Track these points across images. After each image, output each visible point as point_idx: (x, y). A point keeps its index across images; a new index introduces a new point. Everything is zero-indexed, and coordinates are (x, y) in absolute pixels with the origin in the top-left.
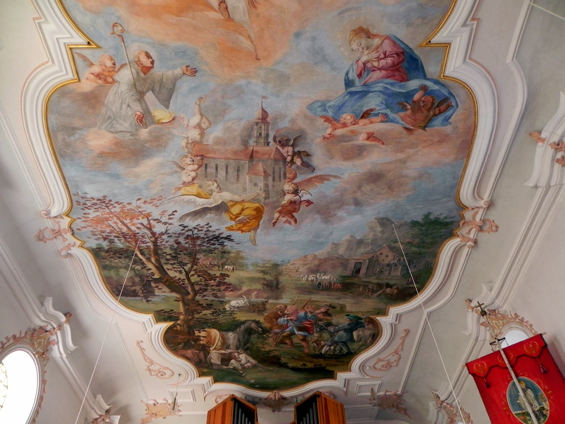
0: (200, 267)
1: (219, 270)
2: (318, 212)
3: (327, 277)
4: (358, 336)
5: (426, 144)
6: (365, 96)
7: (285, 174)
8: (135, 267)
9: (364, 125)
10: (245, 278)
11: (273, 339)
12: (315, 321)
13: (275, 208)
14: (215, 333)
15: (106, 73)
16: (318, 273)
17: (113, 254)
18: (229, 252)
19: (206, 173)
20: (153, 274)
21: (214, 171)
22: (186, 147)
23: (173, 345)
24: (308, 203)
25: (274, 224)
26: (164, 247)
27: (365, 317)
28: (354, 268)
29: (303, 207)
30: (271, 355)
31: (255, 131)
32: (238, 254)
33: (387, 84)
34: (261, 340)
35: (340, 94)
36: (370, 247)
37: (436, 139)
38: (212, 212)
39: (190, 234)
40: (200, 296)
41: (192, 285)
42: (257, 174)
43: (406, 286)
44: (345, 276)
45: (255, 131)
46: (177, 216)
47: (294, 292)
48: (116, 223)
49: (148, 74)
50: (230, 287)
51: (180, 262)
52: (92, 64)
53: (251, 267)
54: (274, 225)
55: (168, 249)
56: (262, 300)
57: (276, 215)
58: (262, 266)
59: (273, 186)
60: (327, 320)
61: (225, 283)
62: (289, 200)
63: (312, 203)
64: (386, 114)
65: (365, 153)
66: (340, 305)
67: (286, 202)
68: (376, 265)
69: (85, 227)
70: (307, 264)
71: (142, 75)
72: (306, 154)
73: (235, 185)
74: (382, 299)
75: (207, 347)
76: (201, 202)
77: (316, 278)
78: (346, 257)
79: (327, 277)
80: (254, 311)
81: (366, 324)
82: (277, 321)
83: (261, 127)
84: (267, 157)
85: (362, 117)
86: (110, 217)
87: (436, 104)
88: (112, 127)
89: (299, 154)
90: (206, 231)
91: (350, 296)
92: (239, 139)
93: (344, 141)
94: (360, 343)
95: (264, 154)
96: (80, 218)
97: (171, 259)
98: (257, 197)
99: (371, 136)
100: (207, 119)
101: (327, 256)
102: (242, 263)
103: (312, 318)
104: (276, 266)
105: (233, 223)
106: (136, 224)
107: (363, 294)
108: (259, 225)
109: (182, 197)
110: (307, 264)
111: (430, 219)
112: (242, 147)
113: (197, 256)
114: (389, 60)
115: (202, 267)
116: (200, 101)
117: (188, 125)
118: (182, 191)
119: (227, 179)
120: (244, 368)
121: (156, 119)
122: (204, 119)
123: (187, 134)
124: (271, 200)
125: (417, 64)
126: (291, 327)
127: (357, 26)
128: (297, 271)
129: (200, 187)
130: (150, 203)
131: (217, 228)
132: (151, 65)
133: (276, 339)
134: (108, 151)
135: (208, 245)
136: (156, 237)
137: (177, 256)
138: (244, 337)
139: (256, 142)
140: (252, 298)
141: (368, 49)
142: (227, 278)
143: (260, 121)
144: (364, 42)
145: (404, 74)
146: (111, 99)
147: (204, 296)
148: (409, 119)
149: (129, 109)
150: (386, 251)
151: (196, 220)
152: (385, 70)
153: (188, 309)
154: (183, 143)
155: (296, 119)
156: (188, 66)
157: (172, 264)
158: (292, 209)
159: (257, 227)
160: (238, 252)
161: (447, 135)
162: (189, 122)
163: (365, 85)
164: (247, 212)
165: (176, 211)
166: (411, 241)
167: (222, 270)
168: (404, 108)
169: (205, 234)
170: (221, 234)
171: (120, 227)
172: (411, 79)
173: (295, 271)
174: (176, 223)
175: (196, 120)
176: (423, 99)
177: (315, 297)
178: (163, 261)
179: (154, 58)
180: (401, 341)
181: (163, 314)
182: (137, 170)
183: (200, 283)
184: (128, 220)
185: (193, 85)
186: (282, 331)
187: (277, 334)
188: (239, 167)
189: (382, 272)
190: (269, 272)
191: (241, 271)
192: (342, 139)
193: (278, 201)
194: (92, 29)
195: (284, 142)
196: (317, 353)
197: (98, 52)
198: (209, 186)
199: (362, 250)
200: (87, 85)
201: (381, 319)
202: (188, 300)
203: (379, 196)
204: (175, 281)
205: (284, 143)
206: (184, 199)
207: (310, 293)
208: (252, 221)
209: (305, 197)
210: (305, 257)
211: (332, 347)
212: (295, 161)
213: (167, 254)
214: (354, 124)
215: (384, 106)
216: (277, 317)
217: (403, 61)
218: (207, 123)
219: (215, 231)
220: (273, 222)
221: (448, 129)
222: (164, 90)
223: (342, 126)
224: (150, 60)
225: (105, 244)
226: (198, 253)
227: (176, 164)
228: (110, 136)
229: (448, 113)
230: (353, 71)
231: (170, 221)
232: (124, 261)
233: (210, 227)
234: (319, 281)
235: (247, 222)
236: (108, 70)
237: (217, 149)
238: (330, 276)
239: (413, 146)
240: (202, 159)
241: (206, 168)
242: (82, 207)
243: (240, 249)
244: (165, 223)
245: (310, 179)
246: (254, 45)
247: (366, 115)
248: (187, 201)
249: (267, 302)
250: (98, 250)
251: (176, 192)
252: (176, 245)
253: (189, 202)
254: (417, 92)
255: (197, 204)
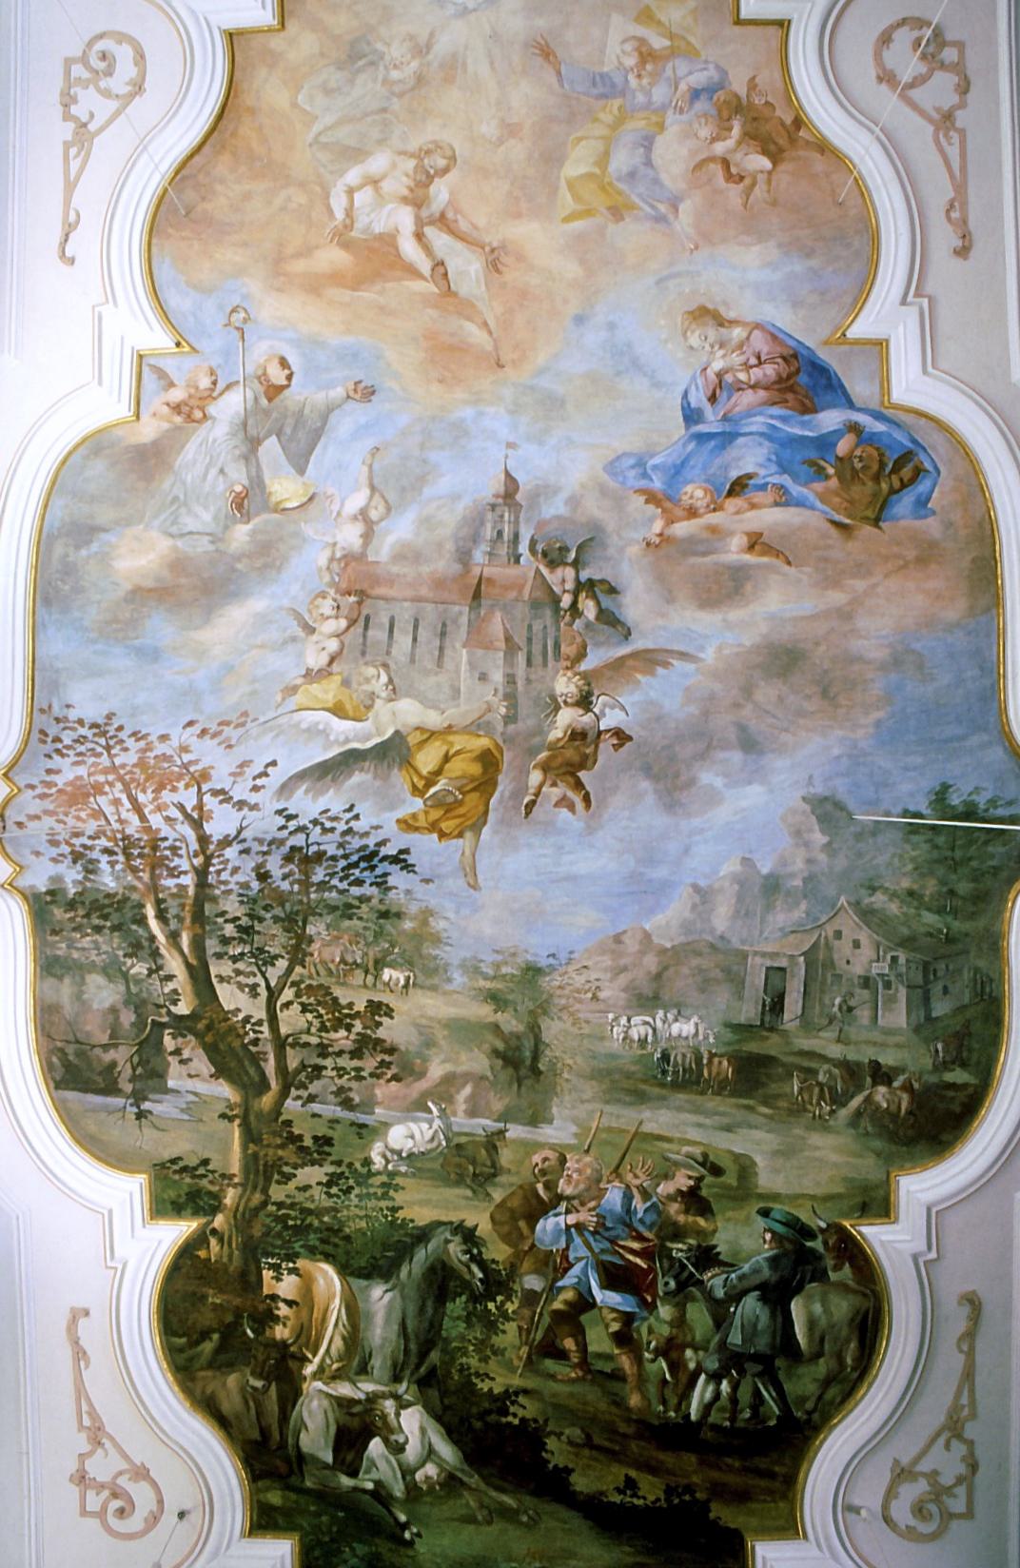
0: (313, 970)
1: (365, 986)
2: (648, 771)
3: (684, 1028)
4: (812, 1324)
5: (890, 566)
6: (731, 442)
7: (557, 646)
8: (133, 966)
9: (738, 513)
10: (439, 1022)
11: (520, 1328)
12: (657, 1236)
13: (532, 752)
14: (327, 1278)
15: (194, 402)
16: (657, 1007)
17: (83, 917)
18: (399, 915)
19: (364, 644)
20: (174, 998)
21: (383, 636)
22: (328, 568)
23: (183, 1340)
24: (619, 739)
25: (530, 807)
26: (224, 892)
27: (823, 1225)
28: (765, 991)
29: (606, 745)
30: (510, 1419)
31: (489, 526)
32: (425, 923)
33: (772, 417)
34: (478, 1335)
35: (676, 437)
36: (803, 906)
37: (911, 554)
38: (367, 764)
39: (298, 845)
40: (299, 1097)
41: (281, 1044)
42: (489, 646)
43: (933, 1079)
44: (740, 1025)
45: (489, 526)
46: (277, 777)
47: (589, 1089)
48: (117, 802)
49: (277, 401)
50: (395, 1063)
51: (258, 949)
52: (172, 385)
53: (459, 979)
54: (527, 814)
55: (233, 897)
56: (487, 1122)
57: (535, 777)
58: (491, 972)
59: (528, 681)
60: (700, 1233)
61: (379, 1041)
62: (569, 726)
63: (630, 738)
64: (782, 487)
65: (748, 587)
66: (737, 1158)
67: (560, 735)
68: (829, 981)
69: (37, 817)
70: (625, 969)
71: (264, 402)
72: (607, 586)
73: (432, 680)
74: (867, 1134)
75: (293, 1356)
76: (346, 733)
77: (654, 1030)
78: (735, 943)
79: (684, 1028)
80: (460, 1181)
81: (830, 1262)
82: (533, 1229)
83: (502, 516)
84: (513, 594)
85: (731, 493)
86: (108, 782)
87: (890, 466)
88: (174, 523)
89: (588, 587)
90: (345, 833)
91: (765, 1116)
92: (450, 546)
93: (695, 554)
94: (822, 1368)
95: (506, 588)
96: (32, 787)
97: (234, 939)
98: (485, 718)
99: (755, 542)
100: (383, 497)
101: (682, 939)
102: (435, 958)
103: (648, 1220)
104: (533, 972)
105: (418, 804)
106: (166, 807)
107: (805, 1110)
108: (486, 813)
109: (297, 716)
110: (625, 969)
111: (949, 805)
112: (457, 568)
113: (310, 930)
114: (770, 370)
115: (318, 974)
116: (373, 455)
117: (339, 514)
118: (299, 699)
119: (413, 661)
120: (413, 1491)
121: (274, 499)
122: (377, 497)
123: (334, 536)
124: (520, 726)
125: (829, 378)
126: (582, 1273)
127: (693, 306)
128: (595, 997)
129: (346, 683)
130: (214, 736)
131: (375, 823)
132: (285, 383)
133: (529, 1331)
134: (149, 583)
135: (344, 885)
136: (208, 853)
137: (252, 927)
138: (422, 1310)
139: (490, 554)
140: (455, 1114)
141: (721, 347)
142: (385, 1020)
143: (500, 501)
144: (712, 333)
145: (806, 397)
146: (190, 456)
147: (312, 1099)
148: (837, 500)
149: (221, 478)
150: (849, 924)
151: (321, 792)
152: (766, 388)
153: (255, 1156)
154: (323, 560)
155: (582, 496)
156: (360, 382)
157: (235, 959)
158: (576, 759)
159: (482, 820)
160: (427, 914)
161: (933, 545)
162: (342, 505)
163: (725, 418)
164: (456, 767)
165: (274, 763)
166: (915, 887)
167: (375, 985)
168: (820, 473)
169: (341, 845)
170: (383, 843)
171: (124, 815)
172: (823, 409)
173: (590, 995)
174: (268, 804)
175: (357, 501)
176: (858, 453)
177: (657, 1119)
178: (212, 945)
179: (294, 369)
180: (959, 1360)
181: (177, 1177)
182: (204, 635)
183: (305, 1038)
184: (149, 791)
185: (363, 420)
186: (551, 1288)
187: (531, 1298)
188: (444, 625)
189: (850, 1009)
190: (510, 997)
191: (429, 993)
192: (690, 547)
193: (540, 731)
194: (191, 319)
195: (555, 555)
196: (672, 1414)
197: (190, 363)
198: (368, 680)
199: (782, 917)
200: (148, 430)
201: (874, 1234)
202: (260, 1115)
203: (801, 721)
204: (232, 1029)
205: (554, 557)
206: (300, 722)
207: (640, 1098)
208: (469, 797)
209: (611, 720)
210: (618, 939)
211: (725, 1386)
212: (580, 606)
213: (227, 917)
214: (715, 510)
215: (774, 468)
216: (537, 1209)
217: (798, 371)
218: (382, 508)
219: (366, 834)
220: (525, 801)
221: (932, 526)
222: (301, 435)
223: (685, 513)
224: (287, 372)
225: (71, 877)
226: (314, 914)
227: (299, 617)
228: (164, 544)
229: (922, 487)
230: (697, 388)
231: (253, 798)
232: (110, 944)
233: (357, 817)
234: (663, 1044)
235: (456, 801)
236: (198, 395)
237: (398, 575)
238: (697, 1024)
239: (861, 570)
240: (360, 603)
241: (366, 627)
242: (49, 747)
243: (433, 903)
244: (241, 804)
245: (622, 659)
246: (495, 340)
247: (737, 488)
248: (308, 730)
249: (501, 1133)
250: (48, 898)
251: (284, 699)
252: (255, 885)
253: (314, 732)
254: (842, 436)
255: (332, 738)
